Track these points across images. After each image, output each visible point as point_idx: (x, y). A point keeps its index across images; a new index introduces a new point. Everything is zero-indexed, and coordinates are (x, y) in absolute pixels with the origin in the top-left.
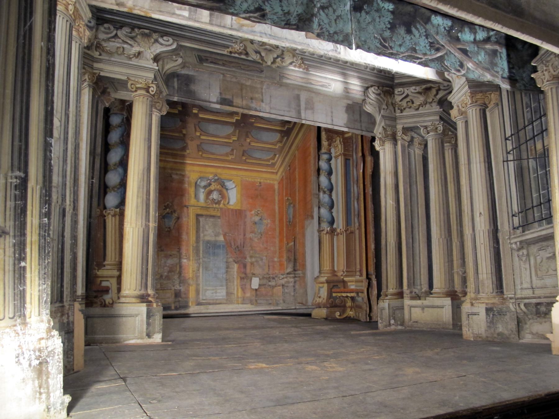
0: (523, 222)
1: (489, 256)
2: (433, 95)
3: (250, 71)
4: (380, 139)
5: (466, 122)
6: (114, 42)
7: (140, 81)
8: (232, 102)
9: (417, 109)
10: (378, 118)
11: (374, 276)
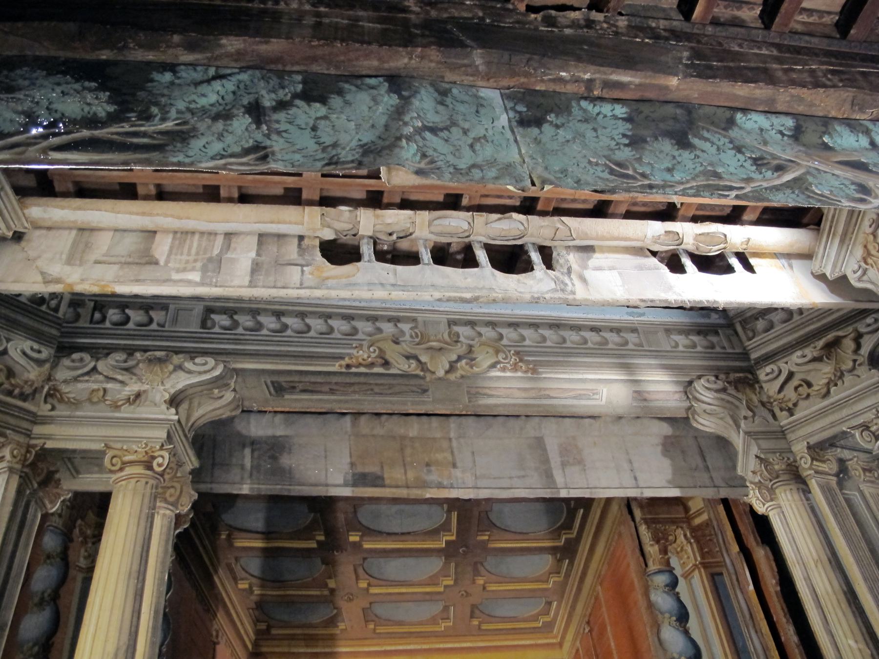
2: (850, 351)
3: (396, 394)
4: (759, 485)
6: (87, 381)
7: (135, 447)
8: (382, 478)
9: (827, 394)
10: (738, 441)
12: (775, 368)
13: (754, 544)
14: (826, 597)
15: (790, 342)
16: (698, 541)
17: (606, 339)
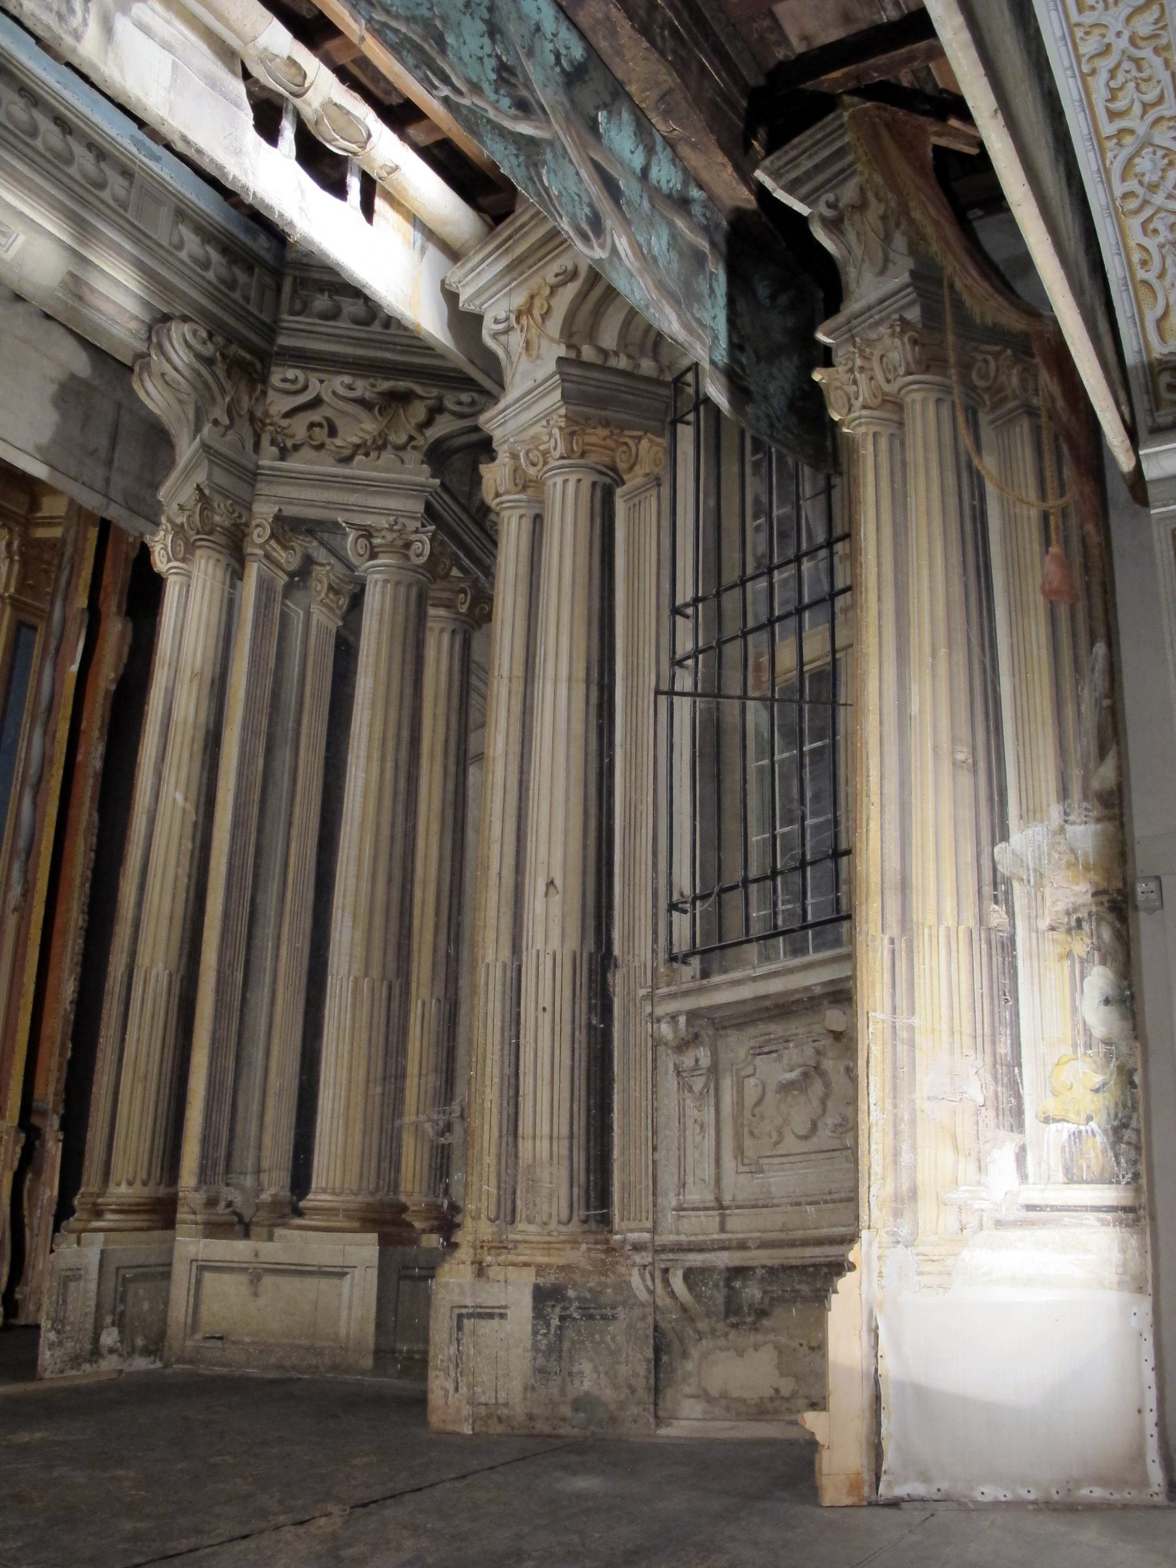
0: (706, 935)
1: (567, 1061)
2: (414, 421)
4: (179, 530)
5: (538, 519)
9: (347, 460)
10: (186, 449)
11: (55, 1121)
12: (302, 380)
13: (114, 609)
14: (180, 730)
15: (345, 356)
16: (24, 563)
17: (71, 153)
